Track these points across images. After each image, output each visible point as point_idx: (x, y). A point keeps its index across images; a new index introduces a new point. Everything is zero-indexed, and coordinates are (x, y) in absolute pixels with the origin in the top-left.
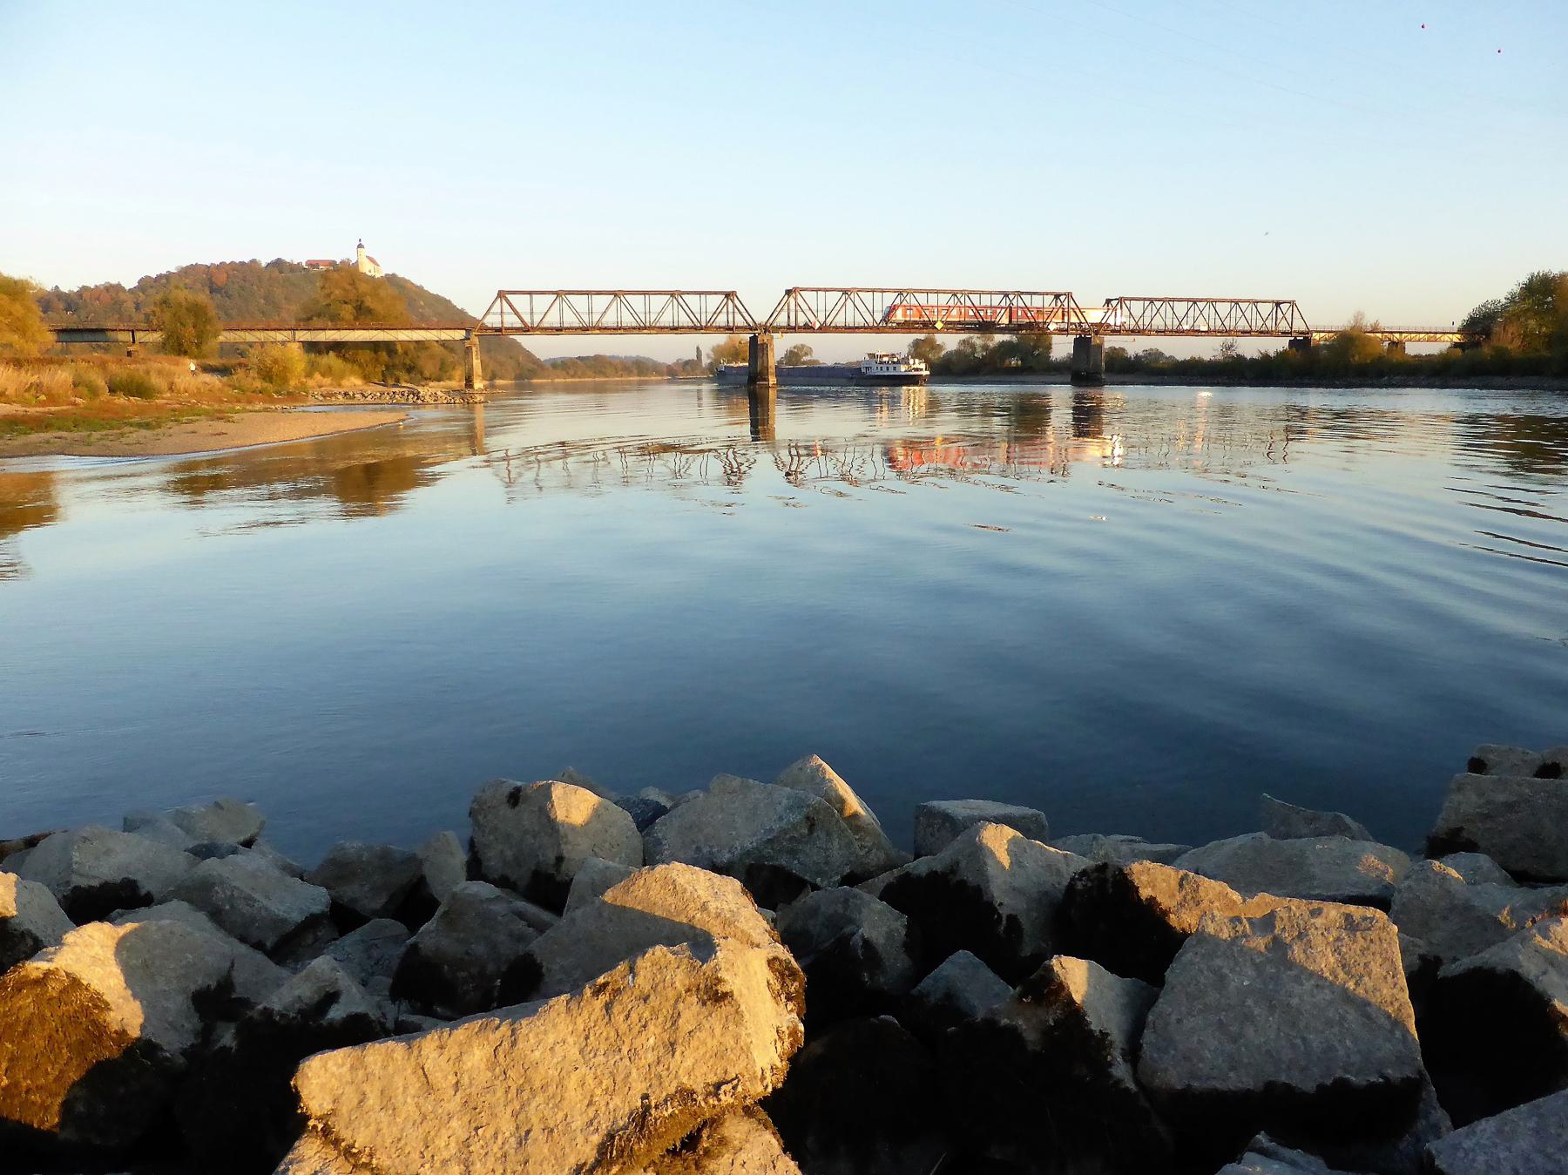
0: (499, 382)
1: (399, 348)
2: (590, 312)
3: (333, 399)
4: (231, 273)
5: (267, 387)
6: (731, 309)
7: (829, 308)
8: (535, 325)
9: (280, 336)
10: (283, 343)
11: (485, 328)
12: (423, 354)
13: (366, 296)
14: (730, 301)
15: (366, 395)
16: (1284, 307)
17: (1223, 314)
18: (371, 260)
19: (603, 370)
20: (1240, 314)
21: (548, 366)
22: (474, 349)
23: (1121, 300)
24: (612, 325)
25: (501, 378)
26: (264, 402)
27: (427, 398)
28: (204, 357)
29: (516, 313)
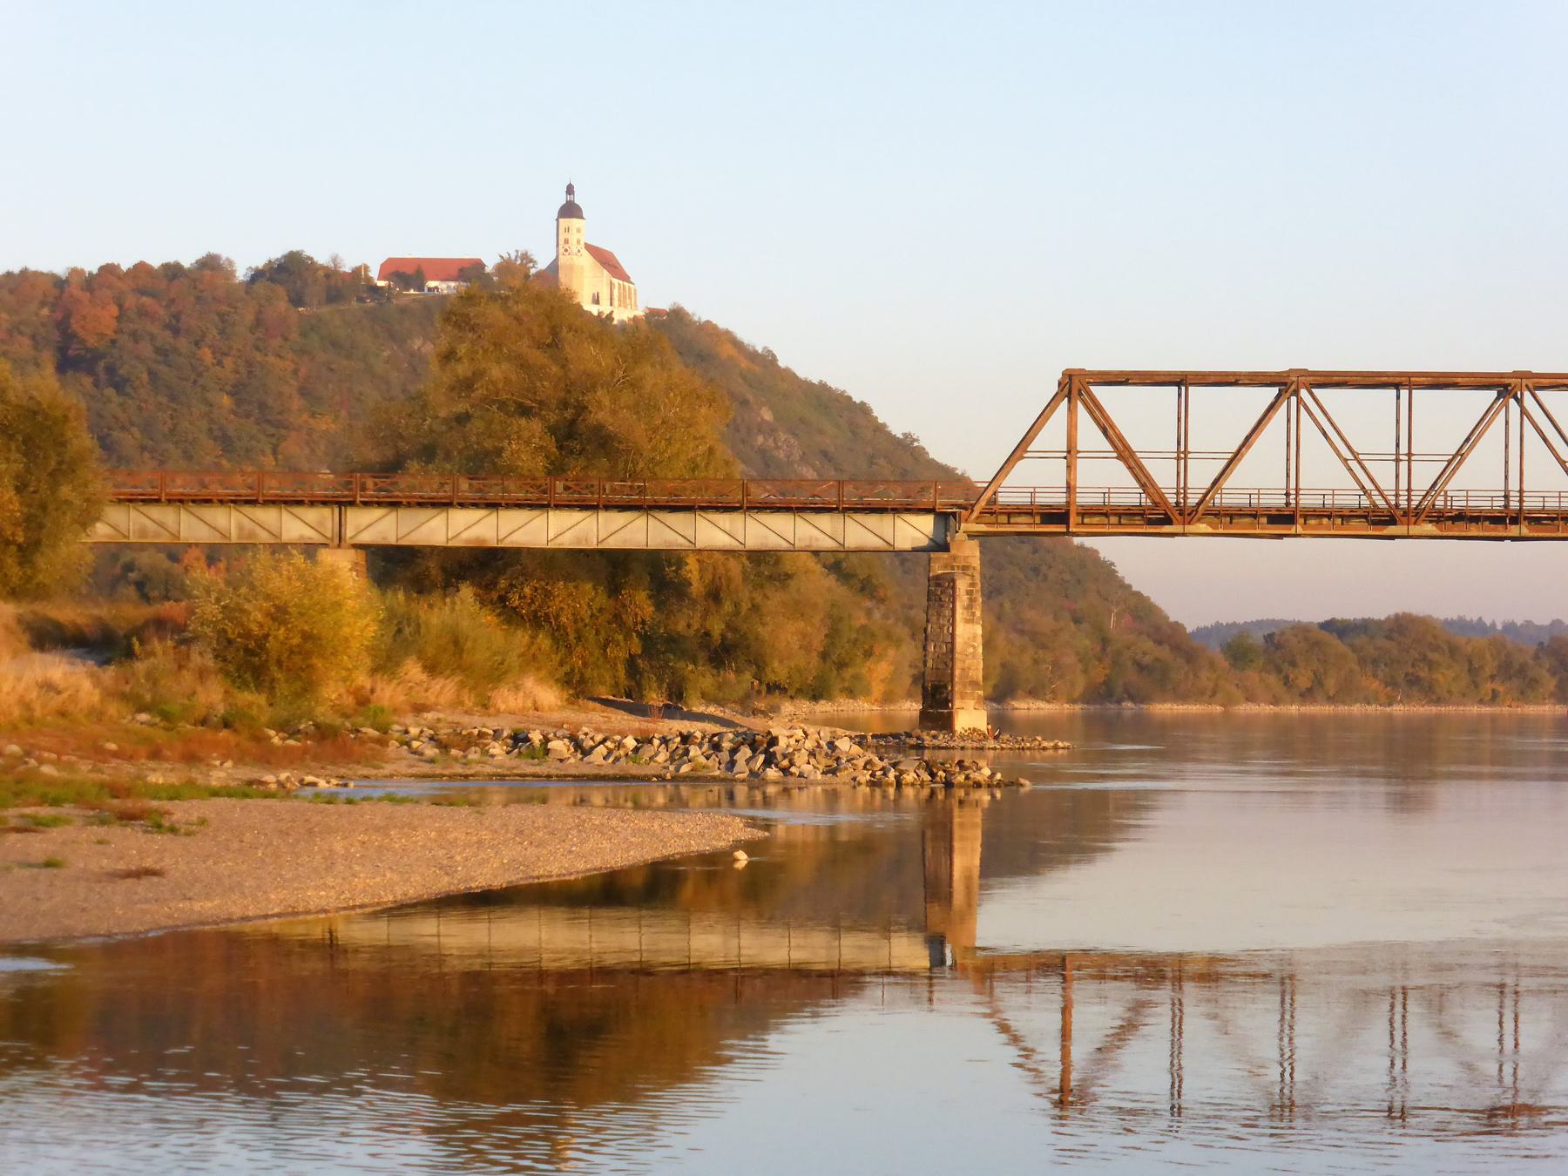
0: (1024, 708)
1: (692, 568)
2: (1404, 456)
3: (473, 754)
4: (131, 301)
5: (250, 705)
8: (1193, 500)
9: (296, 526)
10: (310, 549)
11: (994, 510)
12: (774, 600)
13: (594, 387)
15: (588, 743)
18: (606, 261)
19: (1423, 673)
21: (1215, 651)
22: (962, 585)
24: (1486, 504)
25: (1034, 693)
26: (240, 761)
27: (802, 764)
28: (40, 593)
29: (1125, 453)
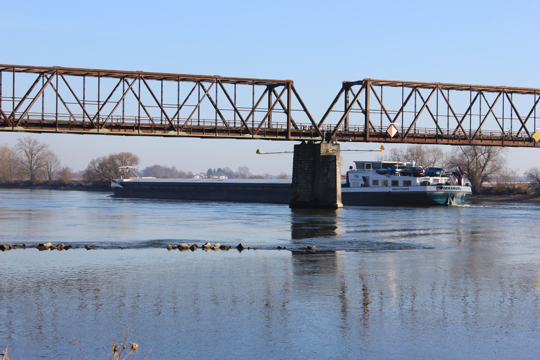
7: (20, 94)
16: (279, 89)
23: (364, 84)
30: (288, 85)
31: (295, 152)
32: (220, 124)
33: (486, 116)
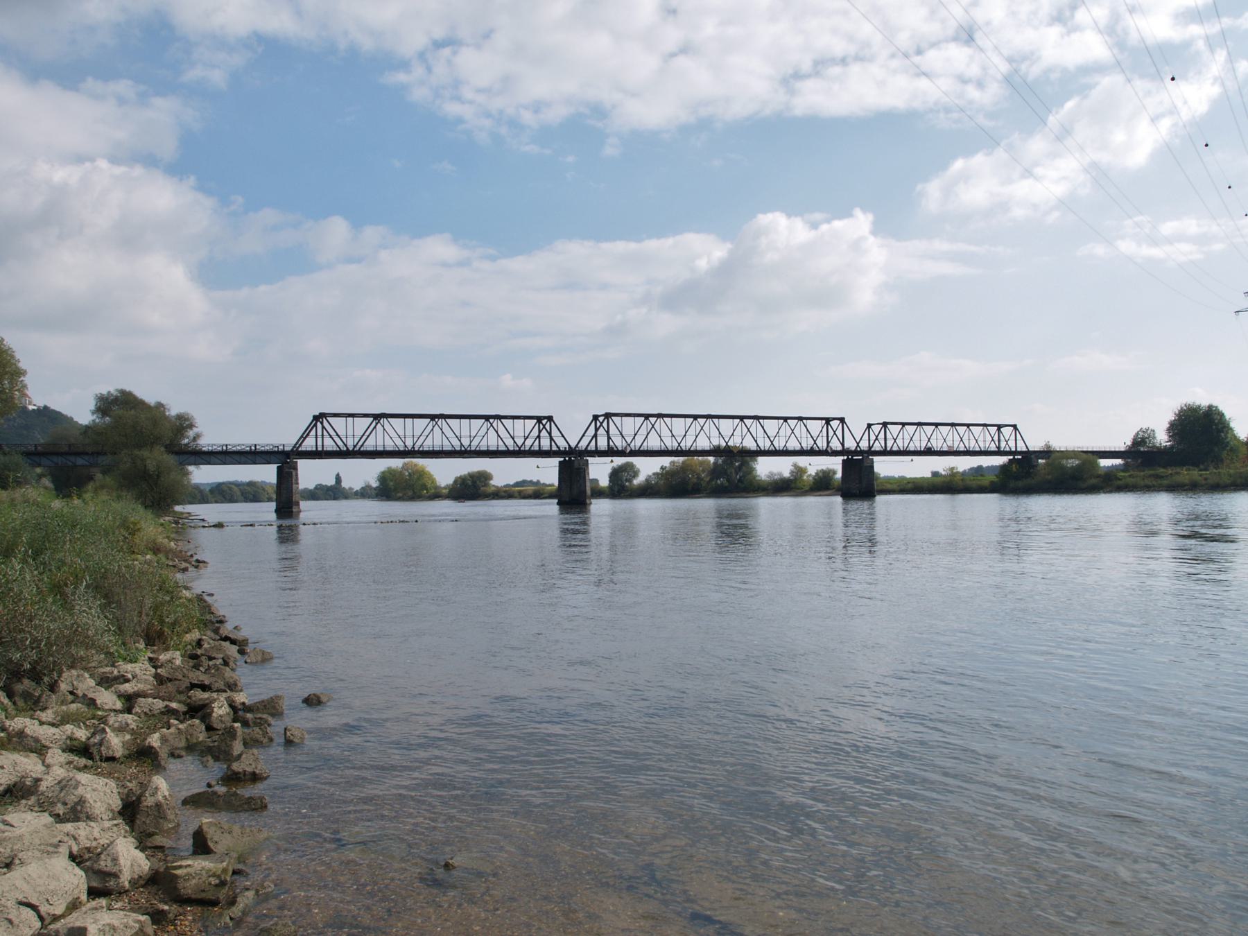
6: (319, 433)
7: (417, 433)
8: (888, 449)
14: (319, 423)
16: (835, 424)
17: (772, 433)
20: (745, 430)
23: (608, 416)
30: (550, 419)
31: (560, 466)
32: (554, 448)
33: (583, 435)
